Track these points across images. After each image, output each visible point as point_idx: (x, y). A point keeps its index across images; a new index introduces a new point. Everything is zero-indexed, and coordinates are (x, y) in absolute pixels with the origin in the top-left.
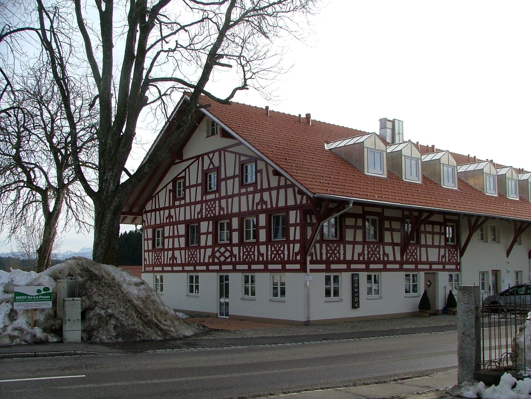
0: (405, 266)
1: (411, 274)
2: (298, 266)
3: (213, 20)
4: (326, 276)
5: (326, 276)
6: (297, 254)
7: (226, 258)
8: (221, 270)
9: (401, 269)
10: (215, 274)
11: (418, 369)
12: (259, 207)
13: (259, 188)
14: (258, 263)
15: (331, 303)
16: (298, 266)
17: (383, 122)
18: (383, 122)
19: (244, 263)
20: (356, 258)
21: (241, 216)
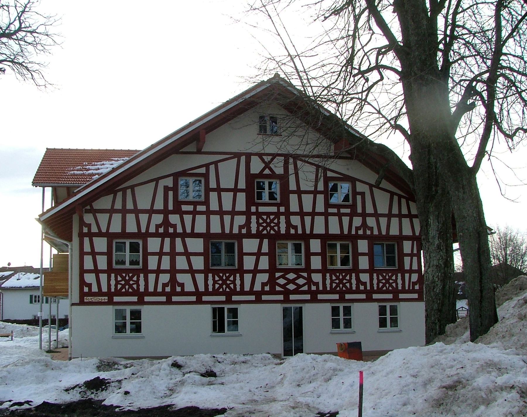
0: (116, 299)
1: (388, 305)
2: (416, 296)
3: (524, 30)
4: (332, 307)
5: (332, 307)
6: (414, 284)
7: (299, 286)
8: (287, 300)
9: (110, 302)
10: (279, 305)
11: (20, 388)
12: (361, 232)
13: (359, 210)
14: (358, 291)
15: (348, 335)
16: (416, 296)
17: (39, 180)
18: (39, 180)
19: (332, 291)
20: (160, 289)
21: (326, 239)
